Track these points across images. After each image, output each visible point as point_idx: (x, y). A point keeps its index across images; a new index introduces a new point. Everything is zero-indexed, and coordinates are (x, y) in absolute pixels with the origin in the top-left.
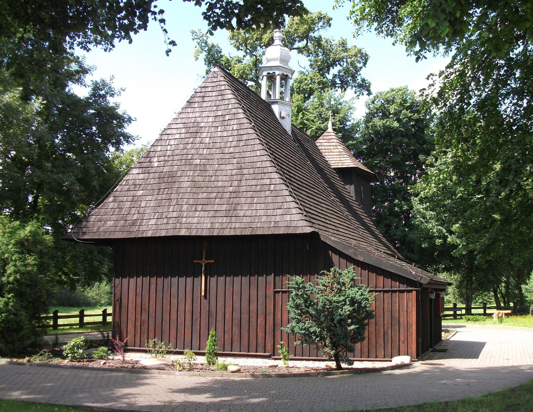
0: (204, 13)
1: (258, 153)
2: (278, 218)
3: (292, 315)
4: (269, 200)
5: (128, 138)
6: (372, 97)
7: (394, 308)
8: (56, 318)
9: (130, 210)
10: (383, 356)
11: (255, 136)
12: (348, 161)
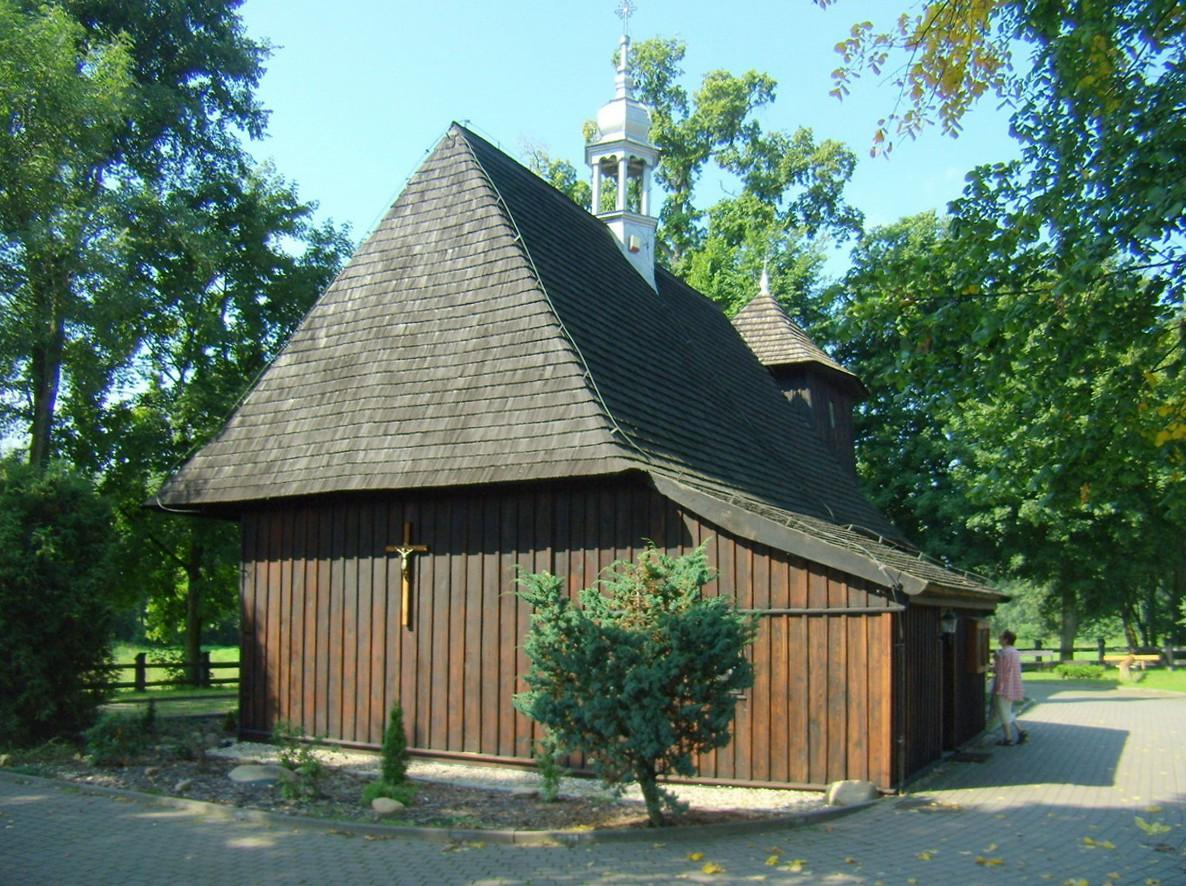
1: (524, 298)
2: (554, 443)
4: (539, 400)
8: (140, 666)
9: (267, 441)
10: (805, 777)
11: (521, 262)
12: (799, 352)
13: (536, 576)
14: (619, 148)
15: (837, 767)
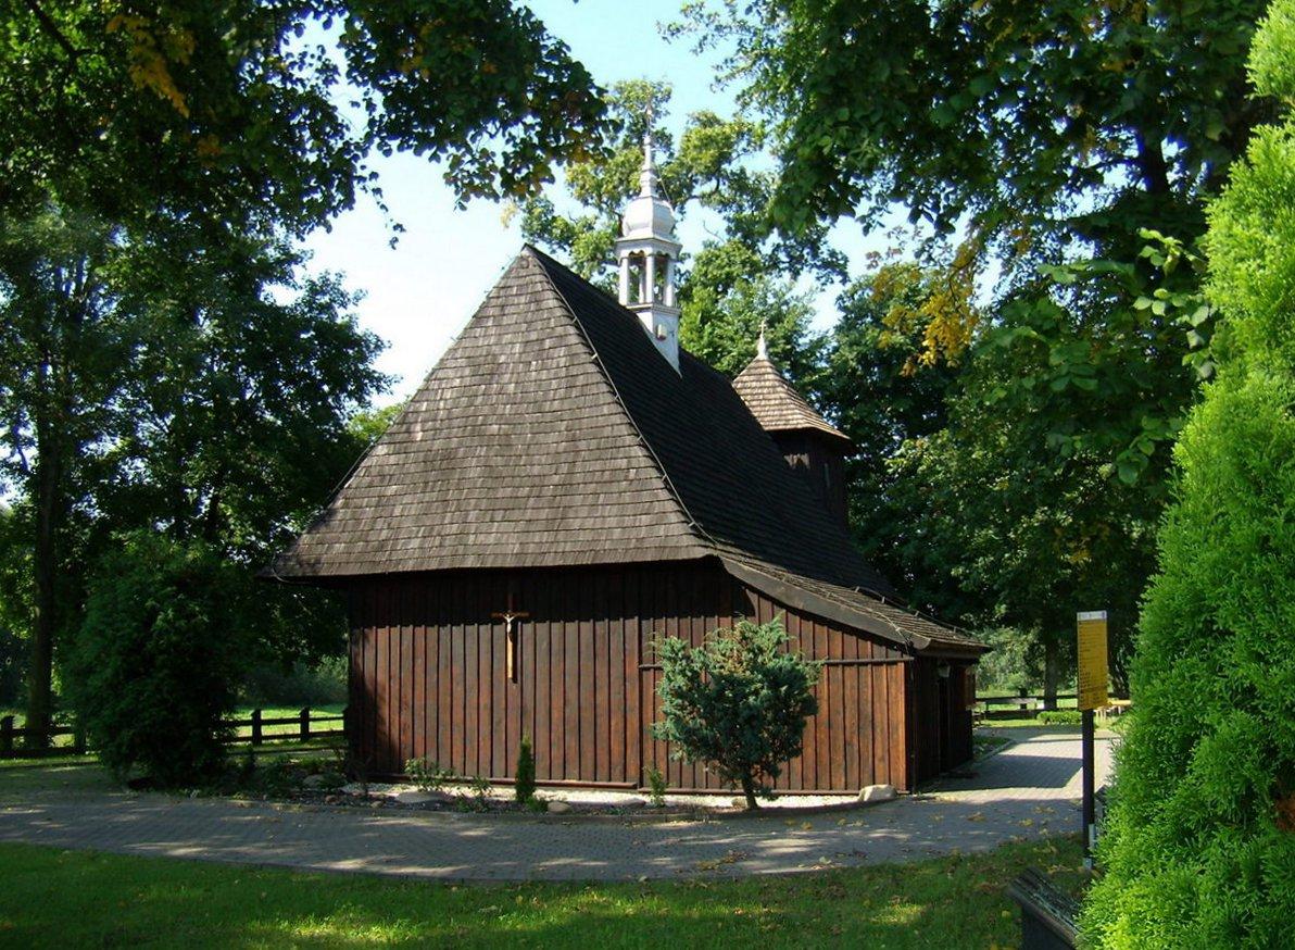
0: (446, 175)
1: (606, 410)
2: (643, 532)
3: (667, 707)
4: (627, 497)
5: (378, 381)
6: (849, 286)
7: (863, 697)
8: (257, 723)
9: (375, 522)
11: (599, 378)
12: (798, 418)
13: (668, 640)
14: (648, 244)
15: (866, 776)
